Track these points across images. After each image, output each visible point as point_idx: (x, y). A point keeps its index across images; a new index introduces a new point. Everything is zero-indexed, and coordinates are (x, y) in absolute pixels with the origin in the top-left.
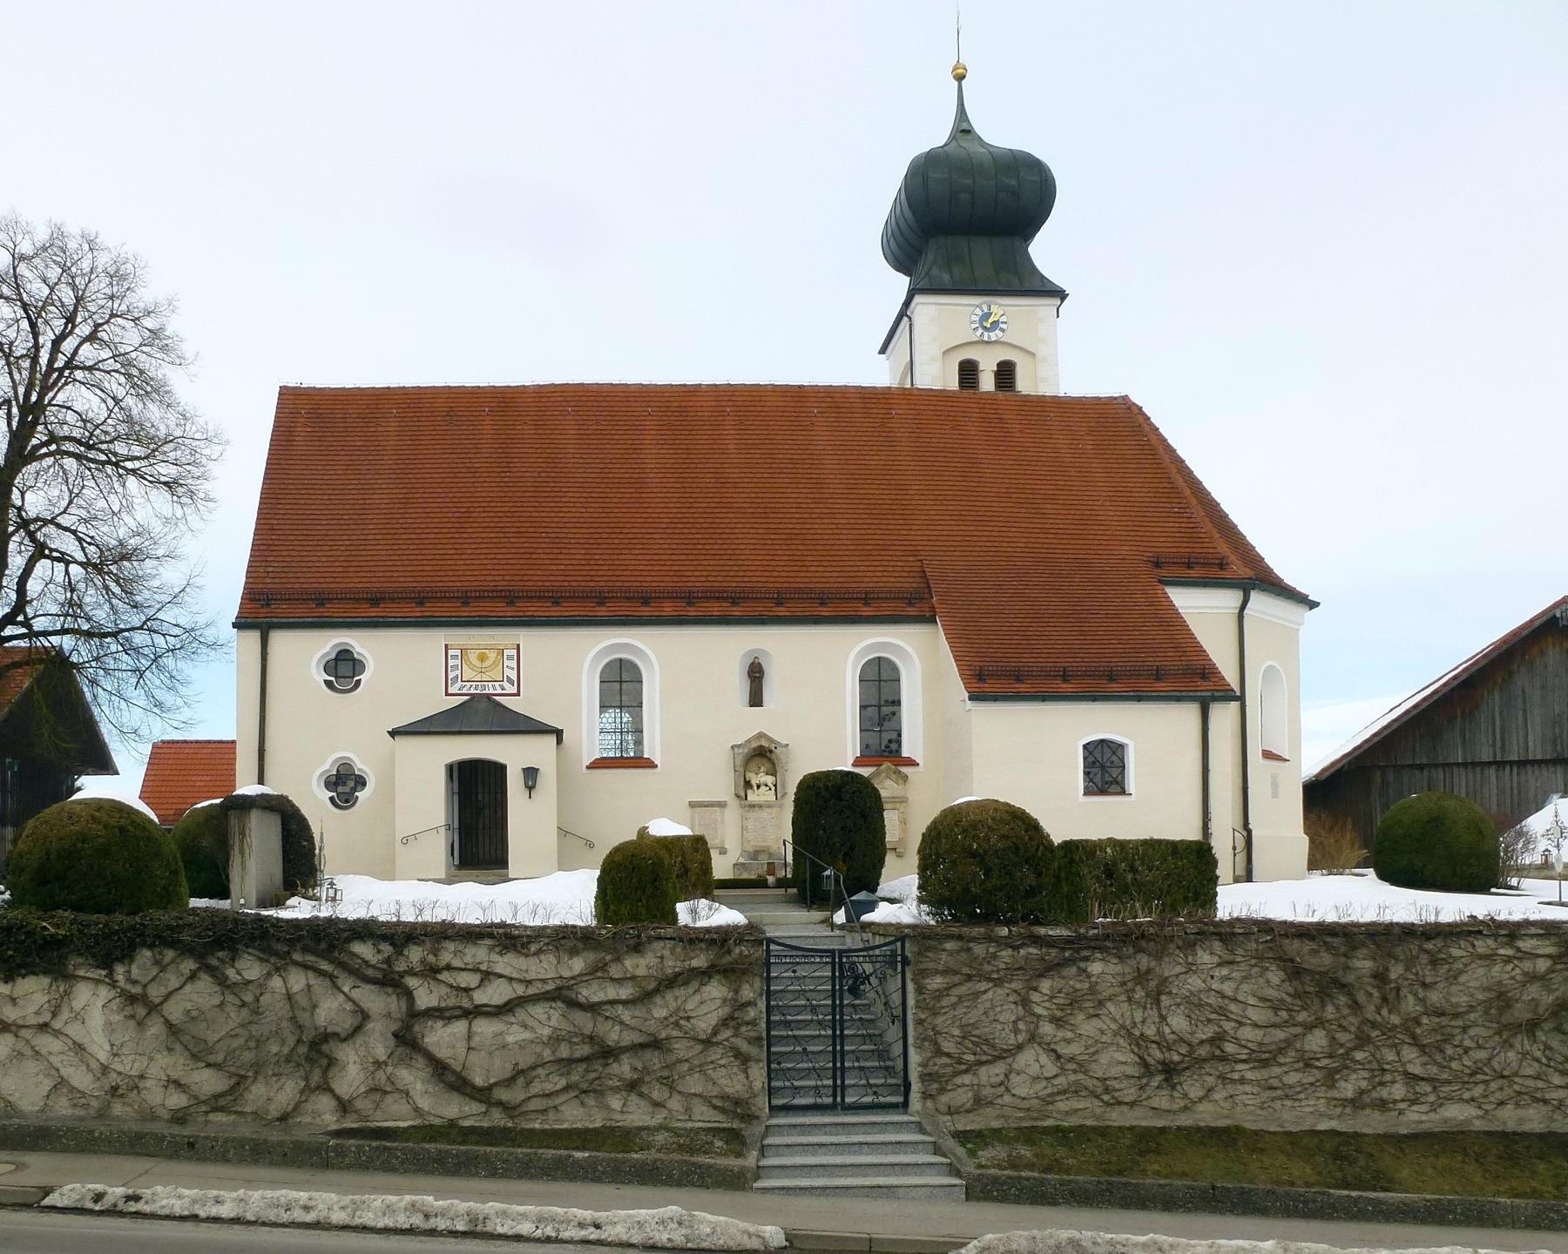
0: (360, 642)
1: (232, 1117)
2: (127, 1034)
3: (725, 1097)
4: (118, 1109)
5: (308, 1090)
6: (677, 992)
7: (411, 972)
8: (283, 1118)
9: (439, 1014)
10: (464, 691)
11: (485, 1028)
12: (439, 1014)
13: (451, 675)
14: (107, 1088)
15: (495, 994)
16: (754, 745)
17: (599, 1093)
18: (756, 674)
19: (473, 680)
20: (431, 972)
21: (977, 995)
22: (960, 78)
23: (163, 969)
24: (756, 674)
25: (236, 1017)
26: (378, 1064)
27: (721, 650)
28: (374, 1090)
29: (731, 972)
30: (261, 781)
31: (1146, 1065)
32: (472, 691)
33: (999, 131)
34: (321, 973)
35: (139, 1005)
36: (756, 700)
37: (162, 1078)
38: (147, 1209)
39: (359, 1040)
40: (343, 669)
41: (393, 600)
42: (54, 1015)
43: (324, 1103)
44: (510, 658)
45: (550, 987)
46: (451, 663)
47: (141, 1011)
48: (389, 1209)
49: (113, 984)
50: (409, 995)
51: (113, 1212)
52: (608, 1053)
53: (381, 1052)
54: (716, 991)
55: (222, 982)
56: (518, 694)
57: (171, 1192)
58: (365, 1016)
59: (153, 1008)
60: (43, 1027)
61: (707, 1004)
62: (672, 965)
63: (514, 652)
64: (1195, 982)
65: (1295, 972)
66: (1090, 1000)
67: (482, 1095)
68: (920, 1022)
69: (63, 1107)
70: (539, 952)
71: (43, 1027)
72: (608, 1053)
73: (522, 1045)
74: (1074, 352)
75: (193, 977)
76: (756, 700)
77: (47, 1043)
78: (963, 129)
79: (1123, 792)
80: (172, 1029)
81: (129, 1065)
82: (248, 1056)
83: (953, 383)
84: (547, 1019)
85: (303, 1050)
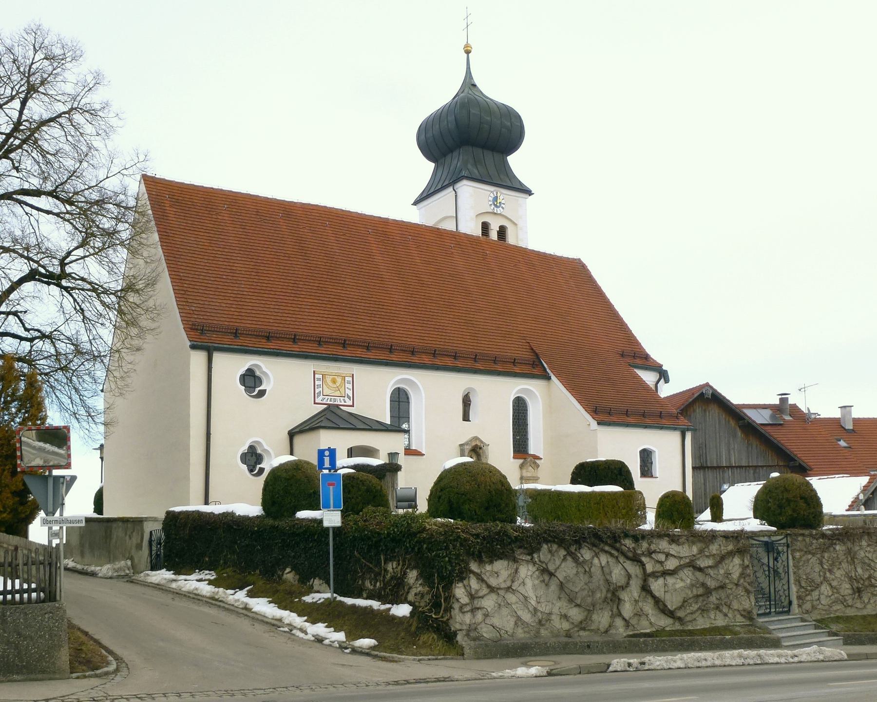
0: (265, 365)
1: (587, 633)
2: (541, 592)
3: (744, 610)
4: (543, 632)
5: (612, 616)
6: (727, 562)
7: (643, 554)
8: (606, 632)
9: (655, 575)
11: (670, 580)
12: (655, 575)
14: (537, 620)
15: (671, 564)
16: (474, 444)
17: (708, 611)
18: (467, 402)
19: (330, 395)
20: (650, 553)
21: (808, 560)
22: (468, 52)
23: (553, 555)
24: (467, 402)
25: (584, 578)
26: (636, 601)
27: (455, 384)
28: (636, 614)
29: (741, 552)
30: (292, 454)
31: (853, 589)
33: (496, 89)
34: (612, 555)
35: (546, 572)
36: (466, 417)
37: (561, 614)
38: (651, 667)
39: (628, 589)
41: (278, 338)
42: (513, 582)
43: (619, 622)
44: (349, 382)
45: (688, 561)
47: (546, 578)
48: (733, 658)
49: (534, 564)
50: (643, 565)
51: (637, 670)
52: (708, 591)
53: (636, 595)
54: (737, 560)
55: (576, 560)
56: (353, 406)
57: (657, 661)
58: (629, 576)
59: (551, 575)
60: (509, 589)
61: (735, 565)
62: (724, 550)
64: (862, 554)
66: (835, 563)
67: (670, 614)
68: (794, 573)
69: (520, 634)
70: (683, 543)
71: (509, 589)
72: (708, 591)
73: (682, 589)
74: (542, 226)
75: (564, 559)
76: (466, 417)
77: (511, 598)
78: (469, 83)
79: (652, 476)
80: (562, 586)
81: (544, 608)
82: (589, 600)
83: (478, 232)
84: (687, 576)
85: (609, 595)
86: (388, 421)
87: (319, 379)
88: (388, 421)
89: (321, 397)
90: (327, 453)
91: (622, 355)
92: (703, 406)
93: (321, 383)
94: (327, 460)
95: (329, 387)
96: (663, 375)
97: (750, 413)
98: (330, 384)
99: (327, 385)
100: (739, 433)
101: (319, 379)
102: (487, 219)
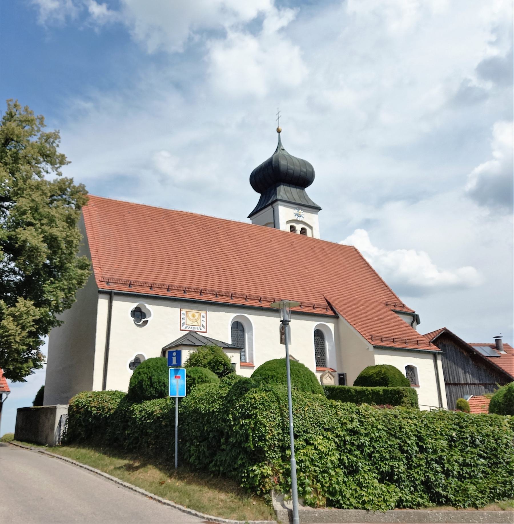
10: (187, 329)
13: (182, 322)
32: (190, 329)
44: (203, 317)
46: (182, 317)
86: (229, 341)
87: (183, 314)
88: (229, 341)
89: (185, 326)
90: (174, 354)
91: (387, 305)
92: (447, 344)
93: (185, 316)
94: (174, 359)
95: (190, 320)
96: (416, 319)
97: (477, 349)
98: (191, 318)
99: (189, 318)
100: (471, 362)
101: (183, 314)
102: (294, 224)
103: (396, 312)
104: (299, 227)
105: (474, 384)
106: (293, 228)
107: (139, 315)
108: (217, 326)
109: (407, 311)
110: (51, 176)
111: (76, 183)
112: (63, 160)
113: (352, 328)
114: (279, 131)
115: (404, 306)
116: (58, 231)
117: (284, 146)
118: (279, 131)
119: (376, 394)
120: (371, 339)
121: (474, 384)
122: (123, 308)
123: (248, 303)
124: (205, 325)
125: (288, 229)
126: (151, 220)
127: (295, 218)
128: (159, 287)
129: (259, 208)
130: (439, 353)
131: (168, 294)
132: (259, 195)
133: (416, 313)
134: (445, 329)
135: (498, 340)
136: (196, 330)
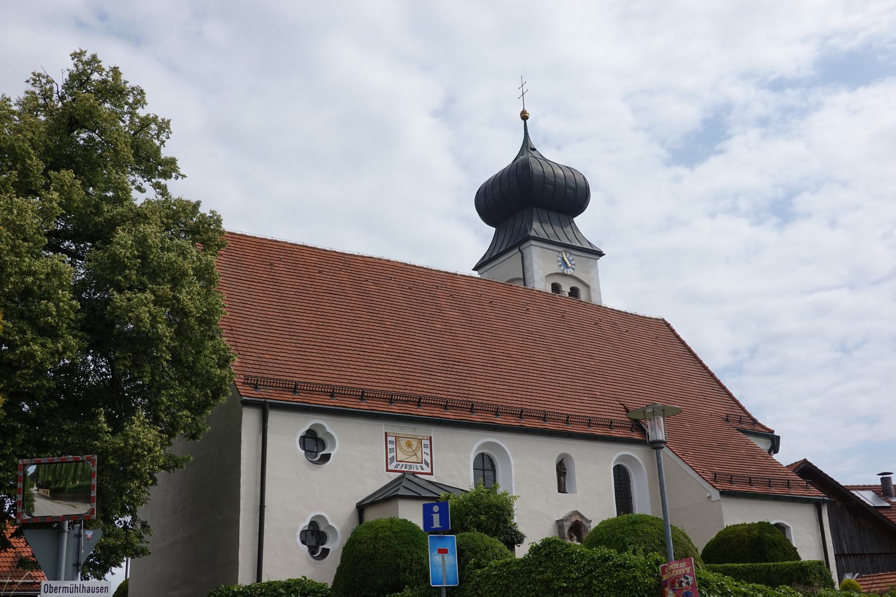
0: (329, 425)
10: (399, 469)
13: (390, 456)
18: (562, 469)
32: (403, 469)
40: (315, 446)
44: (426, 446)
46: (389, 446)
56: (388, 470)
63: (428, 442)
65: (643, 432)
87: (391, 442)
89: (395, 463)
90: (436, 509)
91: (727, 420)
95: (404, 452)
98: (405, 447)
101: (391, 442)
102: (557, 280)
103: (745, 432)
104: (566, 289)
105: (854, 555)
106: (556, 288)
107: (315, 446)
108: (452, 462)
109: (761, 429)
110: (143, 194)
111: (204, 210)
112: (169, 168)
113: (680, 462)
114: (524, 116)
115: (755, 422)
116: (190, 297)
117: (534, 141)
118: (524, 116)
119: (735, 569)
120: (715, 480)
121: (854, 555)
122: (286, 431)
123: (499, 420)
124: (429, 462)
125: (549, 289)
126: (320, 272)
127: (559, 270)
128: (345, 393)
129: (494, 254)
130: (824, 501)
131: (364, 406)
132: (493, 230)
133: (776, 433)
134: (805, 461)
135: (886, 479)
136: (415, 470)
